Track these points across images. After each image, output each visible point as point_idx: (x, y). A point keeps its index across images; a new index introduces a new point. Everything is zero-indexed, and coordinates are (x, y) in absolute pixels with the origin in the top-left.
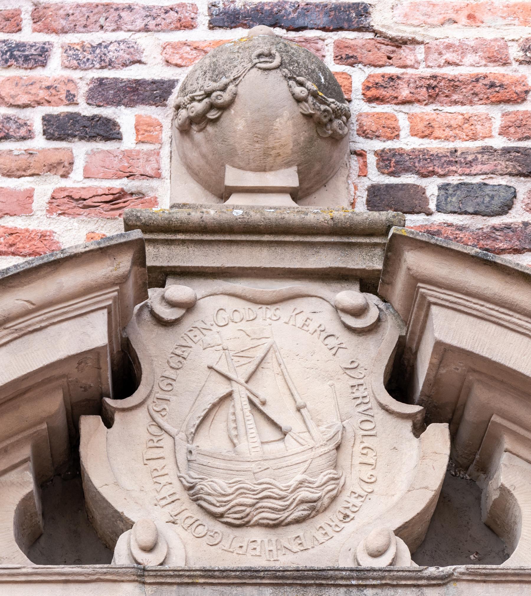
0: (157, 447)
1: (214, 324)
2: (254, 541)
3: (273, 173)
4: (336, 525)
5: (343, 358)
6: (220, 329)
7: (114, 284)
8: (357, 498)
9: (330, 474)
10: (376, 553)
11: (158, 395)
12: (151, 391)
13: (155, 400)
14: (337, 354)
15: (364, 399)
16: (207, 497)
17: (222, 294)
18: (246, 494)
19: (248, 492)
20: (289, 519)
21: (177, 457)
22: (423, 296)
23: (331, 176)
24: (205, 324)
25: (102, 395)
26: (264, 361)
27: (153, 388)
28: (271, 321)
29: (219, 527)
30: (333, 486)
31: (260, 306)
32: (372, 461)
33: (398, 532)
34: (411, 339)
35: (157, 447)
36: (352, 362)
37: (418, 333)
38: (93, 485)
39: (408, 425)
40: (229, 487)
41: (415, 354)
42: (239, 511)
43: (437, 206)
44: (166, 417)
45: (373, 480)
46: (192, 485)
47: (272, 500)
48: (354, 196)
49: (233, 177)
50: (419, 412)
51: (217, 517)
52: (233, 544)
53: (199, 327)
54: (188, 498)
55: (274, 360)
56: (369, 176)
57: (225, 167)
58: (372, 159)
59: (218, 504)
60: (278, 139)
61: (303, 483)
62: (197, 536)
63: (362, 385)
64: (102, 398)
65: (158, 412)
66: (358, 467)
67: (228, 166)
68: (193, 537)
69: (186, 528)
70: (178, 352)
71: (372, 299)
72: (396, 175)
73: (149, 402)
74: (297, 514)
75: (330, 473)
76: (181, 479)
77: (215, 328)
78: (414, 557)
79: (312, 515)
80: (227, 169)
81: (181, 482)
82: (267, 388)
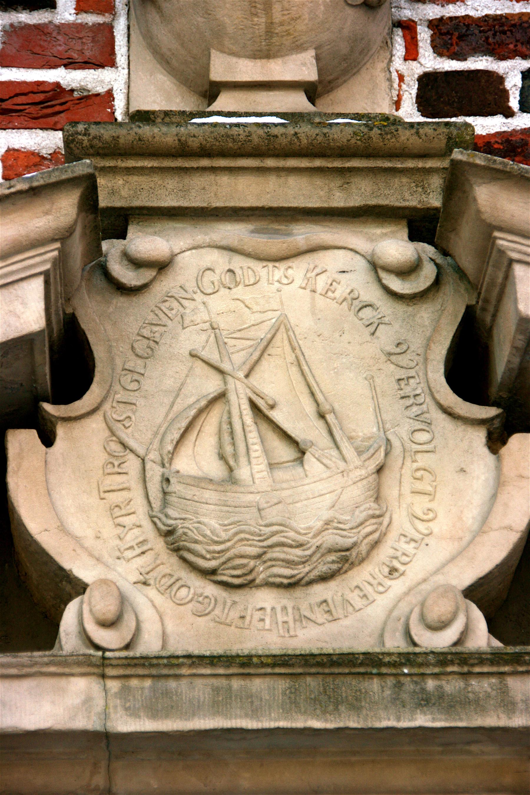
0: (120, 473)
1: (199, 291)
2: (261, 609)
3: (279, 61)
4: (380, 584)
5: (386, 337)
6: (205, 298)
7: (54, 240)
8: (408, 543)
9: (369, 509)
10: (438, 625)
11: (118, 397)
12: (108, 391)
13: (115, 404)
14: (377, 333)
15: (417, 398)
16: (192, 546)
17: (209, 246)
18: (248, 540)
19: (252, 537)
20: (312, 576)
21: (149, 488)
22: (502, 252)
23: (365, 61)
24: (186, 291)
25: (39, 398)
26: (271, 345)
27: (111, 386)
28: (280, 285)
29: (211, 590)
30: (375, 527)
31: (265, 264)
32: (429, 489)
33: (472, 593)
34: (484, 309)
35: (120, 473)
36: (398, 345)
37: (493, 302)
38: (27, 531)
39: (478, 437)
40: (225, 530)
41: (490, 331)
42: (239, 565)
43: (520, 102)
44: (131, 428)
45: (431, 515)
46: (170, 528)
47: (286, 549)
48: (399, 91)
49: (221, 68)
50: (497, 416)
51: (208, 574)
52: (230, 613)
53: (176, 296)
54: (165, 548)
55: (286, 342)
56: (422, 60)
57: (210, 53)
58: (424, 35)
59: (208, 556)
60: (287, 10)
61: (331, 524)
62: (178, 602)
63: (413, 377)
64: (38, 402)
65: (119, 421)
66: (409, 498)
67: (214, 51)
68: (172, 604)
69: (162, 592)
70: (146, 332)
71: (428, 250)
72: (461, 58)
73: (107, 406)
74: (323, 569)
75: (371, 507)
76: (155, 520)
77: (199, 297)
78: (492, 630)
79: (345, 568)
80: (212, 55)
81: (155, 524)
82: (274, 382)
